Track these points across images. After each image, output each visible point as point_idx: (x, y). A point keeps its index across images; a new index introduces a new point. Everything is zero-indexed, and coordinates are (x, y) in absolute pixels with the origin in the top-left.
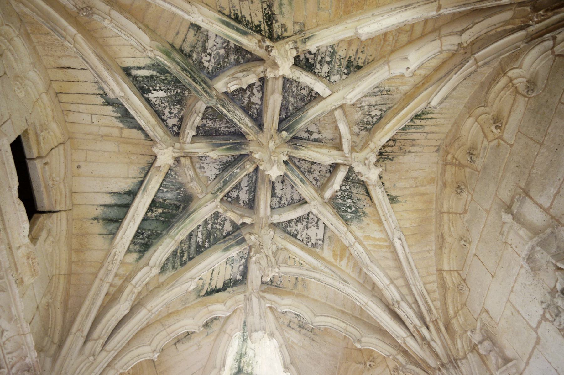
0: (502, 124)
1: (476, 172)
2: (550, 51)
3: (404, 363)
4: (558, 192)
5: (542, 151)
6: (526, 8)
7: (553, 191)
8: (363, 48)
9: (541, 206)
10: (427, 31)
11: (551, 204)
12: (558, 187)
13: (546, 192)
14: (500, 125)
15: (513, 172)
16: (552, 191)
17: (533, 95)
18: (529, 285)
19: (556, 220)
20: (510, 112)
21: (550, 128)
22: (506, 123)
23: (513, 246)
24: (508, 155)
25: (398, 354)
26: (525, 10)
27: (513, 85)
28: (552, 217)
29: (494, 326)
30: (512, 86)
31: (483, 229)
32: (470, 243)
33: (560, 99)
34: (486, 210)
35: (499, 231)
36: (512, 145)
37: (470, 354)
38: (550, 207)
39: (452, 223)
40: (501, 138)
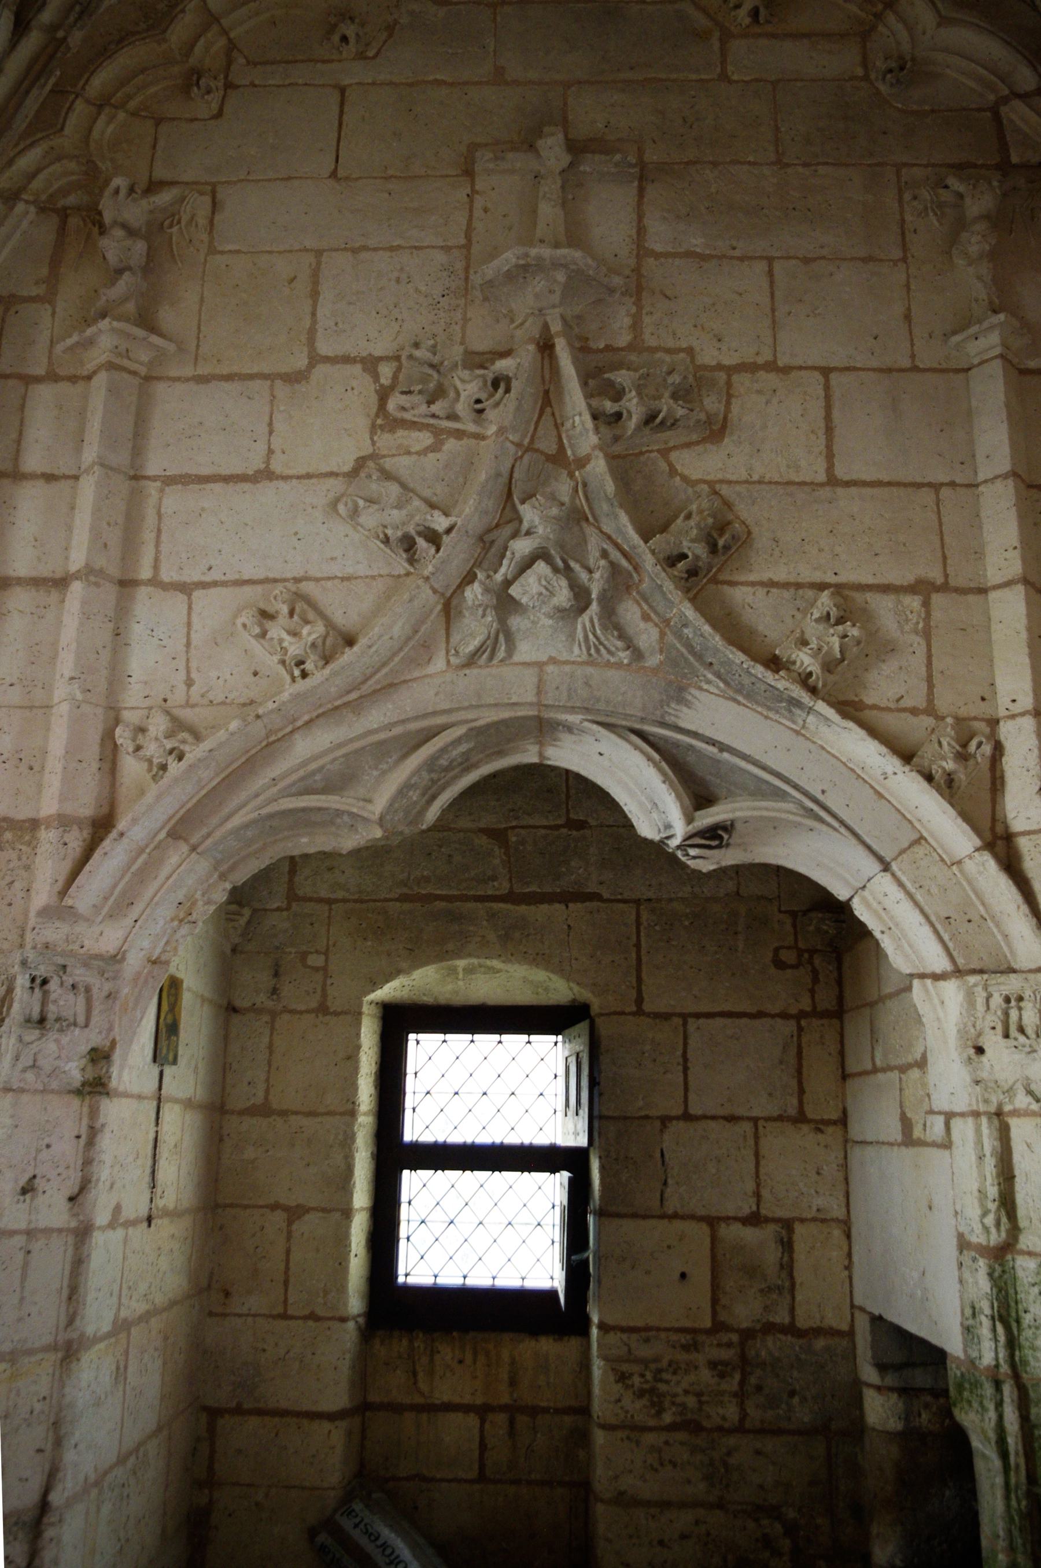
0: (768, 22)
2: (1007, 92)
4: (703, 258)
5: (766, 171)
7: (697, 242)
9: (641, 230)
11: (666, 255)
12: (714, 253)
14: (761, 20)
16: (694, 241)
17: (883, 88)
18: (417, 290)
22: (774, 36)
23: (479, 202)
24: (694, 77)
27: (878, 16)
30: (875, 15)
31: (438, 83)
32: (361, 56)
33: (905, 165)
36: (724, 77)
40: (726, 36)
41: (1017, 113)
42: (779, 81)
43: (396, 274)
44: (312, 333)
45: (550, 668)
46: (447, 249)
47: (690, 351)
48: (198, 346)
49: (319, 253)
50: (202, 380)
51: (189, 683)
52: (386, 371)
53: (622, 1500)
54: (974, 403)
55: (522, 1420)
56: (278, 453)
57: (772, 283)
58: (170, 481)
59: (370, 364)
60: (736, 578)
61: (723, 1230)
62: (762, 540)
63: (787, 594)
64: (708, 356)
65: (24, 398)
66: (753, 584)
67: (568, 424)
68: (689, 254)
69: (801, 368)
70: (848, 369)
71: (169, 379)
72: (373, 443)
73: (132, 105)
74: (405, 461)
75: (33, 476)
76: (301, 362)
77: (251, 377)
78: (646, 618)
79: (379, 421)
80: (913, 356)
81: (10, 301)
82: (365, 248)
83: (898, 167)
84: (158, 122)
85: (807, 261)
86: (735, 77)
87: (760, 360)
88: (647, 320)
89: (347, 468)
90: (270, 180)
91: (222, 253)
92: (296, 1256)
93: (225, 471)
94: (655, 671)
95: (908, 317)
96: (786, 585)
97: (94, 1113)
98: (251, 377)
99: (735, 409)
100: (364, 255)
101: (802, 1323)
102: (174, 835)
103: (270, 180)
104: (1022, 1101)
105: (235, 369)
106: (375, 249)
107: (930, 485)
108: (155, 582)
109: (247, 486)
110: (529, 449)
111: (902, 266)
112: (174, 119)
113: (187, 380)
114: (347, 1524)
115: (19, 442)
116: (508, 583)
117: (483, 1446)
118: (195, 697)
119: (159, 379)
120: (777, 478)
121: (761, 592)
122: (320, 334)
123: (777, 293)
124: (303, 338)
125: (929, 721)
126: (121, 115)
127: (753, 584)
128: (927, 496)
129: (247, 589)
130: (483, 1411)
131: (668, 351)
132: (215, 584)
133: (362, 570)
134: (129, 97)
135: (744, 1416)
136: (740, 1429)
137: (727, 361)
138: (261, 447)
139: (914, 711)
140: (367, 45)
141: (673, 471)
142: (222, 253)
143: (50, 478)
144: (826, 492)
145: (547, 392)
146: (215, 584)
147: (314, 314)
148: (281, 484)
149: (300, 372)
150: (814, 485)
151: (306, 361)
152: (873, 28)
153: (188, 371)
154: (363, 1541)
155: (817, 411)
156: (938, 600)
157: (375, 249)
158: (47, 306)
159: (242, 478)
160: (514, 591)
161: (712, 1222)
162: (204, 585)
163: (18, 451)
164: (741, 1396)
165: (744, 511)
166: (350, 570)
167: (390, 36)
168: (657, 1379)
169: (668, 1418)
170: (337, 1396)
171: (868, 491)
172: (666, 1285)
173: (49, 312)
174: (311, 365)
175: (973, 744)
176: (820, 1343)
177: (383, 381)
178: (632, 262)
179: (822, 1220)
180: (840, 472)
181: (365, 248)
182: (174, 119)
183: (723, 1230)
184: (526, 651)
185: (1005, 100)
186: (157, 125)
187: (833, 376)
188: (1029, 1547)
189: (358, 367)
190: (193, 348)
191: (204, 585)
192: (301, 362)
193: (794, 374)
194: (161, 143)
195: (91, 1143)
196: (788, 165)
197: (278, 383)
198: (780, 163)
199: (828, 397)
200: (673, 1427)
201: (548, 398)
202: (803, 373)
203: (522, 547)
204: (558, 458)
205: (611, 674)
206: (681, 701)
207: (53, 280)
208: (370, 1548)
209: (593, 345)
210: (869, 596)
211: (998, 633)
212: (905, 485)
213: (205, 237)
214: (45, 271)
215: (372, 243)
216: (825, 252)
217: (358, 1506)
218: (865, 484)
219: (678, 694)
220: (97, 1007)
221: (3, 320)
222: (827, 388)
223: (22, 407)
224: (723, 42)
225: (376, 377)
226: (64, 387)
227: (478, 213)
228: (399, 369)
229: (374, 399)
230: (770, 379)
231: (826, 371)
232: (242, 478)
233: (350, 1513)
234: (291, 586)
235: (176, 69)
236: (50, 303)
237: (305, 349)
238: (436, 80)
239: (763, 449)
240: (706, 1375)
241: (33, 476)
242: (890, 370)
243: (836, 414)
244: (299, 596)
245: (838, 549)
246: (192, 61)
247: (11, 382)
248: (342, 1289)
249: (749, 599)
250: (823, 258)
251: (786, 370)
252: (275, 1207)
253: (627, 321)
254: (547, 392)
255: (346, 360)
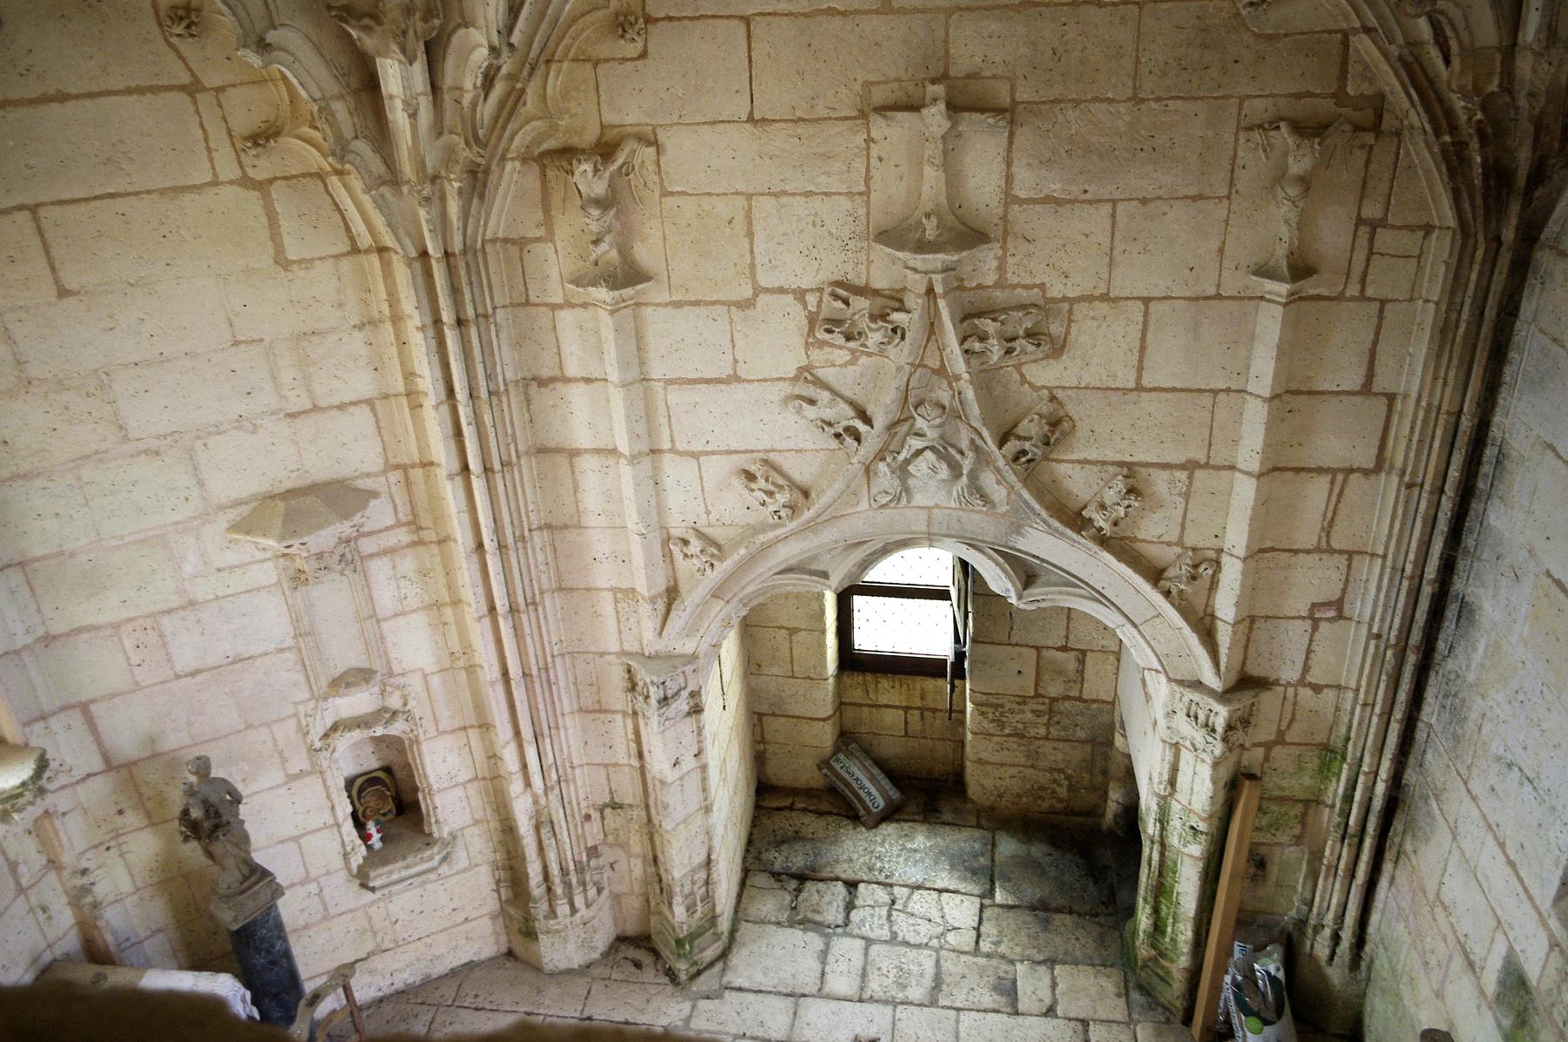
3: (349, 134)
4: (1058, 202)
6: (1496, 82)
7: (1055, 188)
9: (1009, 179)
13: (1044, 172)
15: (1034, 44)
21: (1180, 102)
23: (875, 151)
25: (341, 97)
26: (1490, 74)
28: (1004, 218)
29: (650, 184)
33: (1249, 96)
35: (871, 78)
37: (517, 164)
38: (1022, 202)
45: (935, 511)
46: (850, 194)
47: (1042, 286)
50: (678, 305)
51: (708, 513)
52: (812, 299)
53: (980, 761)
54: (1258, 329)
55: (927, 714)
58: (669, 382)
59: (800, 294)
60: (1062, 457)
61: (1045, 653)
62: (1082, 431)
63: (1095, 469)
64: (1056, 291)
66: (1072, 462)
68: (1049, 200)
69: (1128, 299)
74: (832, 370)
75: (576, 380)
78: (998, 482)
80: (1219, 285)
85: (1144, 201)
87: (1096, 294)
88: (1010, 260)
89: (791, 375)
92: (795, 652)
94: (1004, 515)
95: (1221, 251)
96: (1096, 463)
97: (698, 721)
99: (1073, 332)
100: (784, 200)
101: (1085, 697)
102: (714, 596)
104: (1188, 744)
106: (793, 194)
107: (1211, 391)
108: (673, 450)
111: (1225, 202)
113: (667, 305)
114: (837, 767)
116: (907, 462)
117: (906, 723)
118: (713, 521)
120: (1098, 385)
121: (1078, 467)
123: (1117, 233)
124: (747, 272)
125: (1178, 550)
126: (565, 65)
127: (1072, 462)
128: (1207, 400)
129: (735, 456)
130: (906, 709)
131: (1025, 287)
132: (714, 453)
133: (809, 445)
134: (568, 48)
135: (1049, 733)
136: (1046, 738)
137: (1071, 295)
139: (1169, 544)
141: (1024, 380)
144: (1133, 396)
146: (714, 453)
148: (746, 385)
150: (1125, 391)
153: (666, 298)
154: (846, 776)
155: (1135, 332)
157: (793, 194)
159: (719, 381)
160: (911, 468)
161: (1038, 649)
162: (706, 453)
164: (1047, 725)
165: (1071, 408)
166: (801, 446)
168: (1002, 715)
169: (1007, 731)
170: (827, 710)
171: (1164, 395)
172: (1012, 674)
174: (756, 295)
175: (1203, 567)
176: (1095, 706)
178: (1000, 211)
179: (1104, 651)
181: (785, 193)
183: (1045, 653)
184: (919, 499)
185: (1355, 31)
186: (595, 66)
191: (706, 453)
194: (602, 87)
195: (699, 734)
196: (1143, 100)
198: (1136, 100)
199: (1145, 323)
200: (1009, 735)
201: (932, 329)
202: (1130, 303)
204: (941, 371)
205: (974, 516)
206: (1019, 533)
207: (548, 222)
208: (850, 780)
209: (967, 284)
210: (1151, 470)
211: (1235, 500)
212: (1192, 391)
213: (656, 178)
214: (540, 216)
216: (1161, 193)
217: (841, 756)
219: (1017, 529)
220: (689, 678)
221: (753, 1038)
222: (1146, 314)
226: (578, 311)
227: (874, 162)
230: (1103, 307)
231: (1146, 301)
232: (719, 381)
233: (838, 760)
234: (762, 455)
239: (1096, 355)
240: (1029, 715)
241: (576, 380)
243: (1150, 336)
244: (766, 462)
248: (825, 667)
250: (1159, 198)
251: (1117, 300)
252: (781, 627)
253: (995, 263)
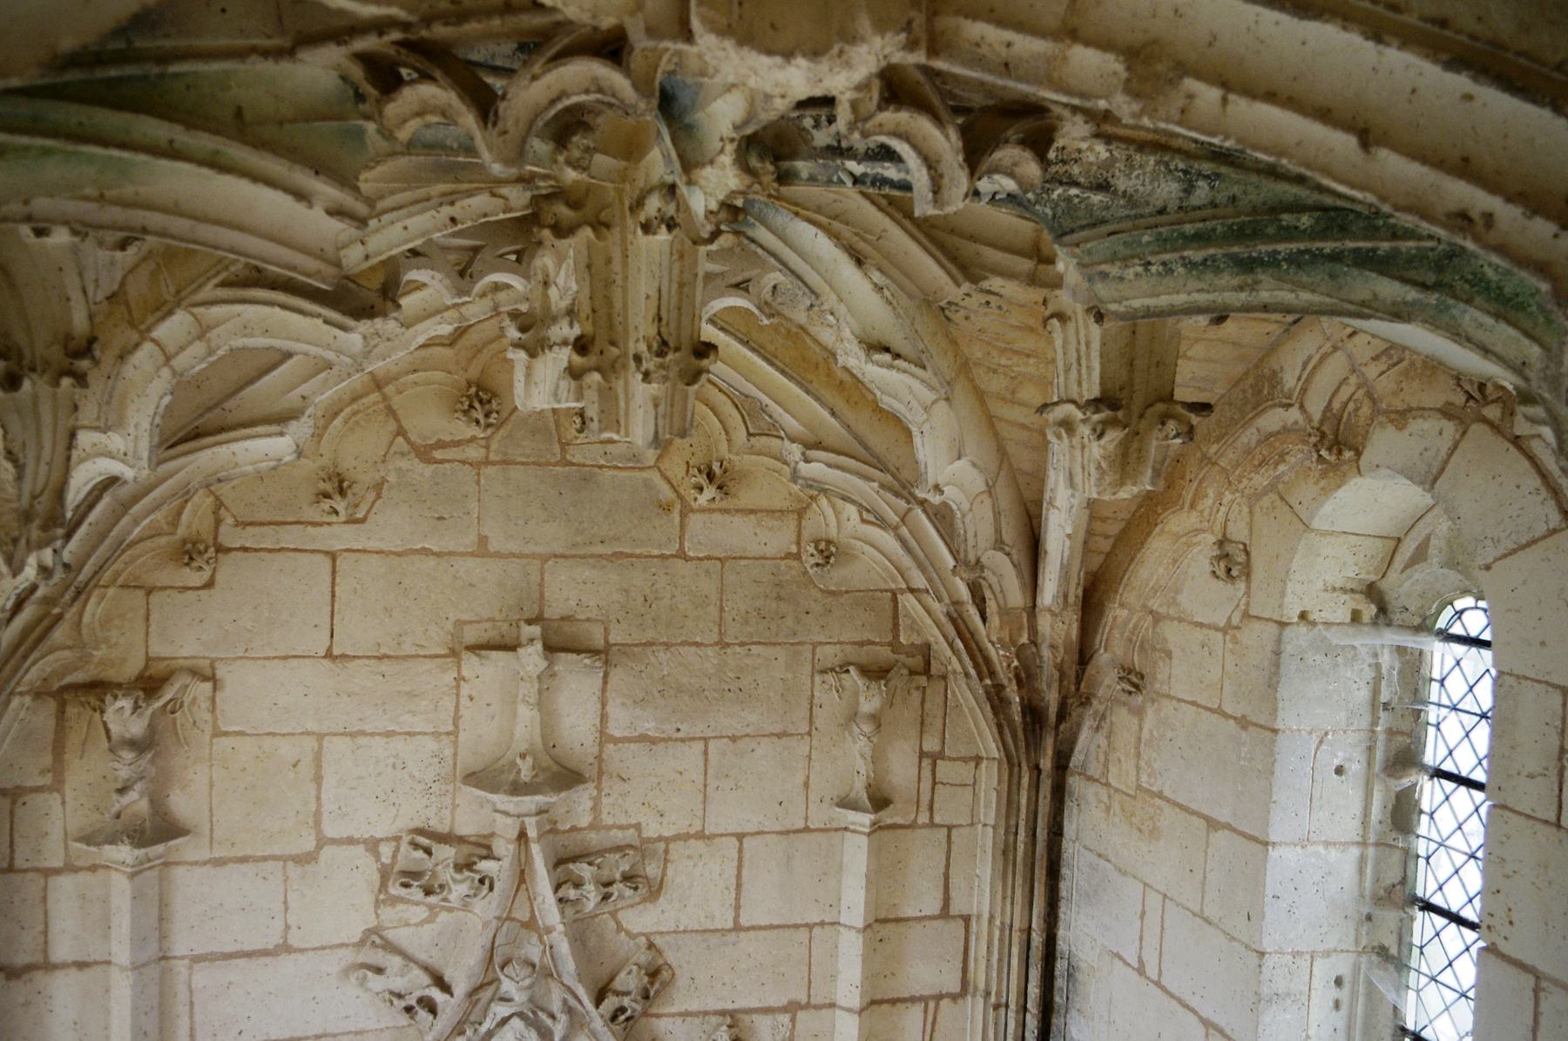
1: (557, 449)
7: (649, 727)
8: (1000, 308)
9: (604, 718)
10: (1000, 427)
13: (638, 712)
16: (647, 725)
18: (412, 776)
19: (600, 768)
20: (752, 511)
22: (726, 511)
23: (465, 690)
28: (599, 758)
31: (425, 552)
34: (483, 540)
35: (465, 617)
37: (28, 699)
38: (616, 741)
39: (355, 413)
41: (908, 602)
42: (727, 558)
43: (392, 760)
44: (318, 815)
46: (436, 735)
48: (212, 830)
49: (321, 737)
50: (219, 862)
52: (386, 851)
54: (845, 860)
56: (294, 929)
57: (706, 760)
58: (196, 959)
62: (682, 981)
63: (697, 1021)
64: (651, 831)
65: (45, 889)
66: (673, 1015)
67: (540, 899)
68: (643, 738)
70: (758, 833)
71: (186, 863)
72: (378, 916)
73: (120, 581)
76: (309, 844)
77: (265, 859)
79: (382, 897)
81: (14, 795)
82: (363, 733)
83: (815, 646)
84: (150, 591)
86: (691, 554)
87: (692, 831)
88: (605, 800)
89: (356, 939)
90: (268, 658)
91: (226, 734)
93: (248, 947)
95: (806, 785)
98: (265, 859)
99: (670, 872)
100: (362, 740)
103: (268, 658)
105: (249, 852)
106: (372, 734)
107: (806, 925)
109: (268, 960)
110: (509, 918)
112: (166, 588)
115: (45, 933)
119: (178, 863)
120: (696, 927)
121: (679, 1020)
122: (325, 817)
123: (710, 771)
124: (311, 821)
126: (111, 592)
127: (673, 1015)
131: (621, 827)
133: (372, 1025)
137: (666, 834)
138: (279, 924)
140: (356, 506)
141: (620, 928)
142: (226, 734)
143: (81, 965)
144: (732, 937)
145: (522, 872)
147: (318, 798)
148: (299, 956)
149: (309, 853)
150: (723, 932)
151: (314, 843)
152: (809, 506)
153: (205, 855)
156: (801, 1015)
157: (372, 734)
158: (56, 795)
159: (265, 953)
163: (46, 943)
165: (670, 957)
166: (361, 1026)
167: (379, 496)
173: (59, 801)
174: (319, 847)
177: (384, 860)
180: (744, 921)
181: (363, 733)
182: (166, 588)
185: (902, 592)
187: (745, 840)
188: (1270, 290)
189: (361, 848)
190: (207, 832)
192: (309, 844)
193: (716, 841)
194: (154, 617)
196: (728, 645)
197: (290, 863)
198: (723, 644)
199: (740, 859)
201: (522, 877)
203: (502, 1010)
204: (531, 924)
207: (58, 769)
209: (561, 827)
213: (208, 716)
214: (47, 759)
215: (368, 728)
216: (749, 731)
218: (761, 928)
223: (45, 899)
224: (683, 515)
225: (377, 856)
226: (83, 877)
227: (464, 701)
228: (397, 849)
229: (376, 877)
230: (698, 845)
231: (740, 837)
232: (265, 953)
235: (163, 540)
236: (58, 791)
237: (313, 832)
238: (424, 549)
242: (788, 832)
243: (745, 873)
245: (737, 982)
246: (181, 531)
247: (30, 875)
249: (670, 1027)
253: (590, 804)
254: (522, 872)
255: (351, 841)
